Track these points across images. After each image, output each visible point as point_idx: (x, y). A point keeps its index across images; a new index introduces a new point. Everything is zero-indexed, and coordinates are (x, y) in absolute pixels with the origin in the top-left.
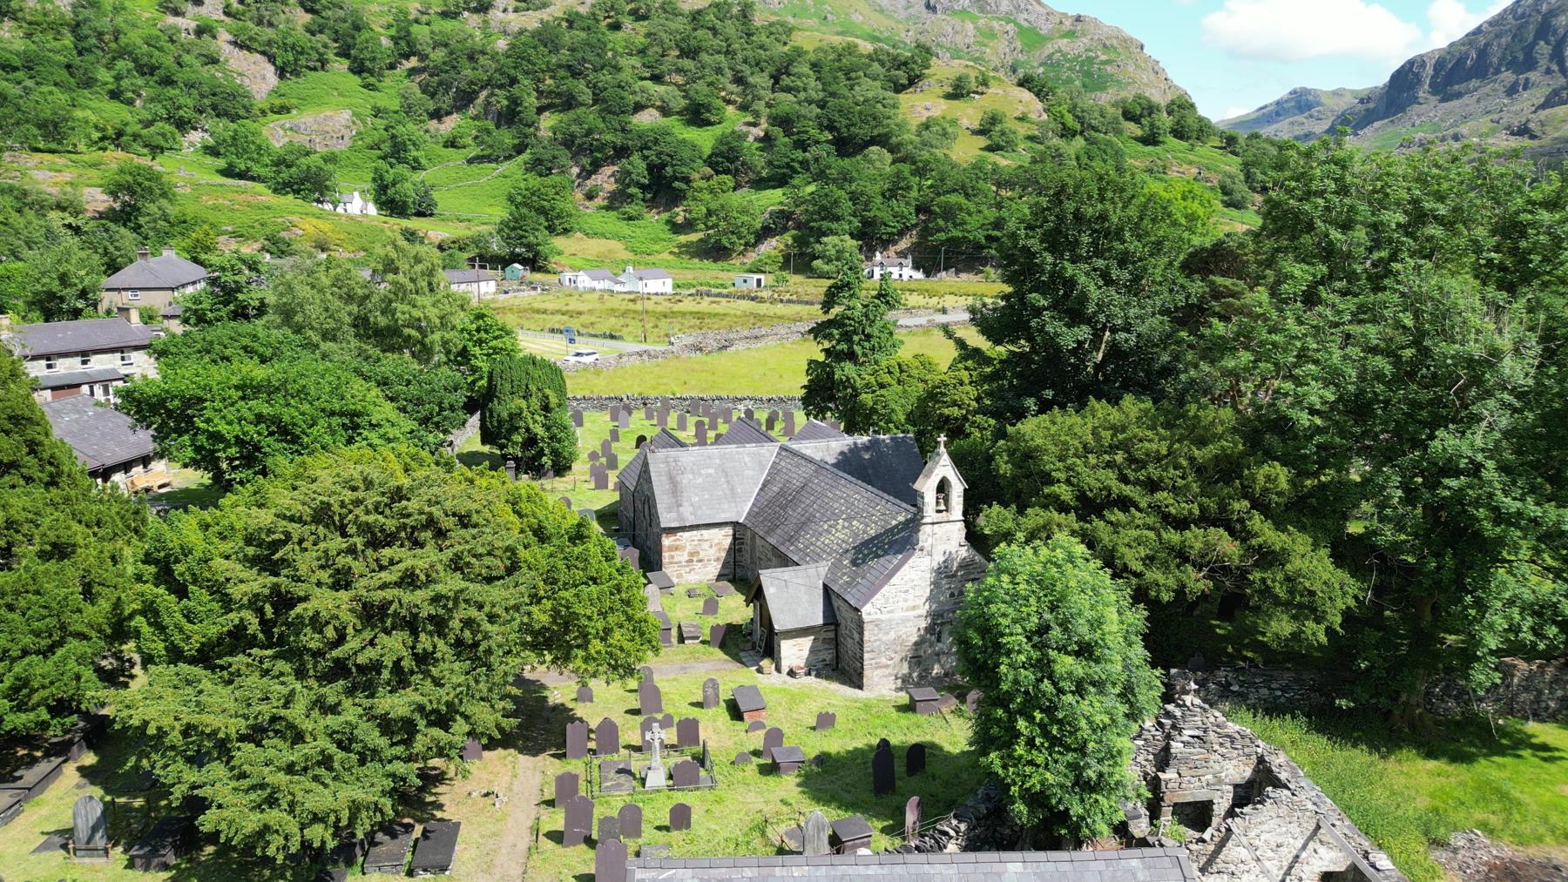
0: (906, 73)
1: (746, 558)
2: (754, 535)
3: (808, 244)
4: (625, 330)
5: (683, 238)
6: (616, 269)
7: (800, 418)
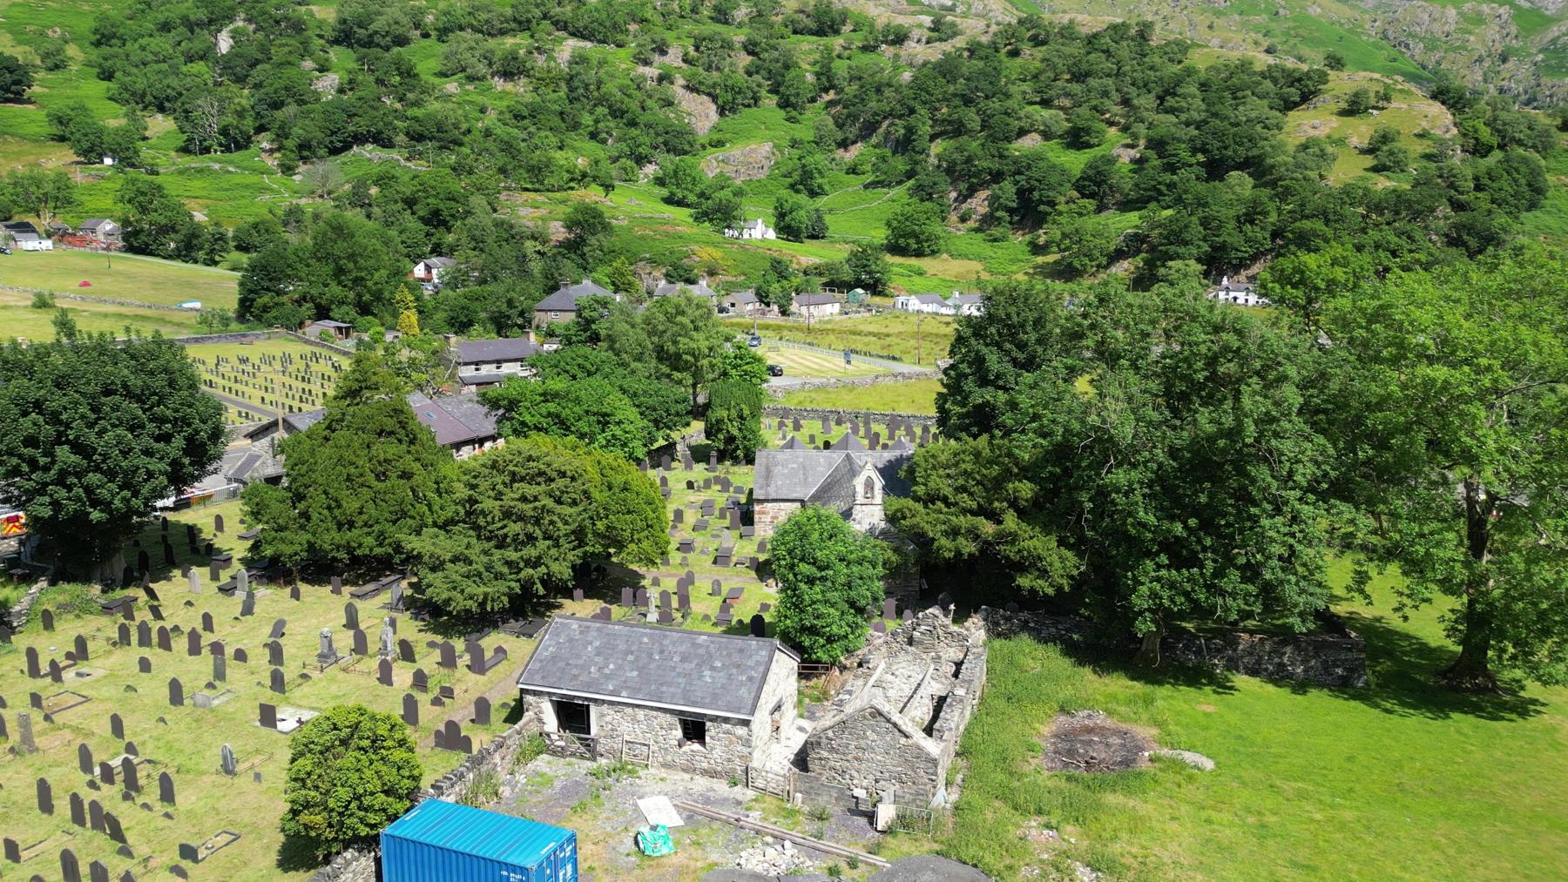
0: (1299, 91)
5: (1040, 260)
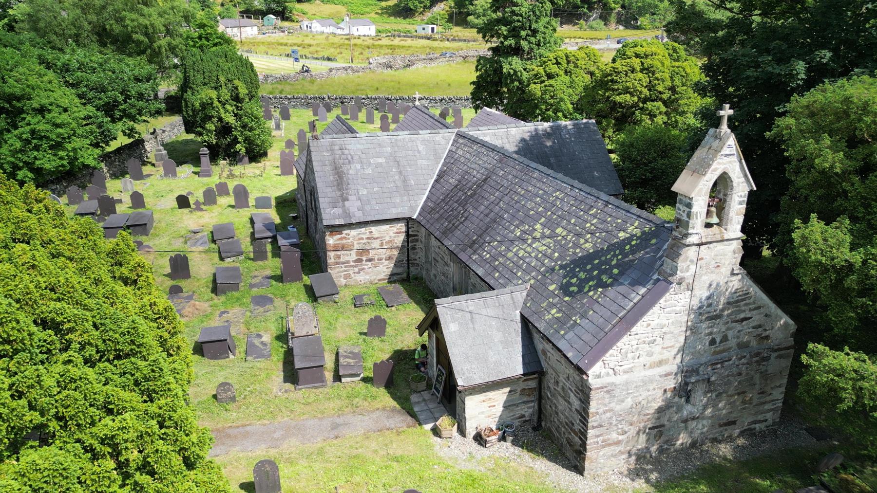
1: (420, 256)
2: (429, 233)
3: (464, 6)
4: (340, 56)
6: (336, 20)
7: (468, 113)
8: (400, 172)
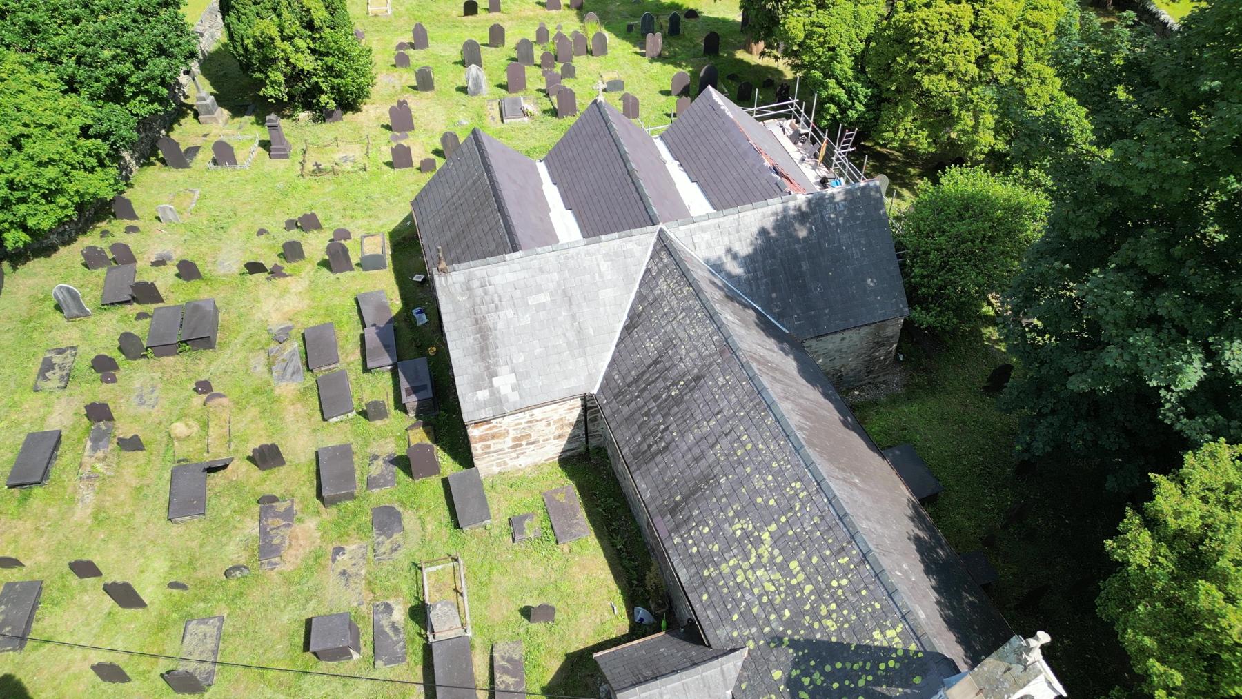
8: (573, 316)
